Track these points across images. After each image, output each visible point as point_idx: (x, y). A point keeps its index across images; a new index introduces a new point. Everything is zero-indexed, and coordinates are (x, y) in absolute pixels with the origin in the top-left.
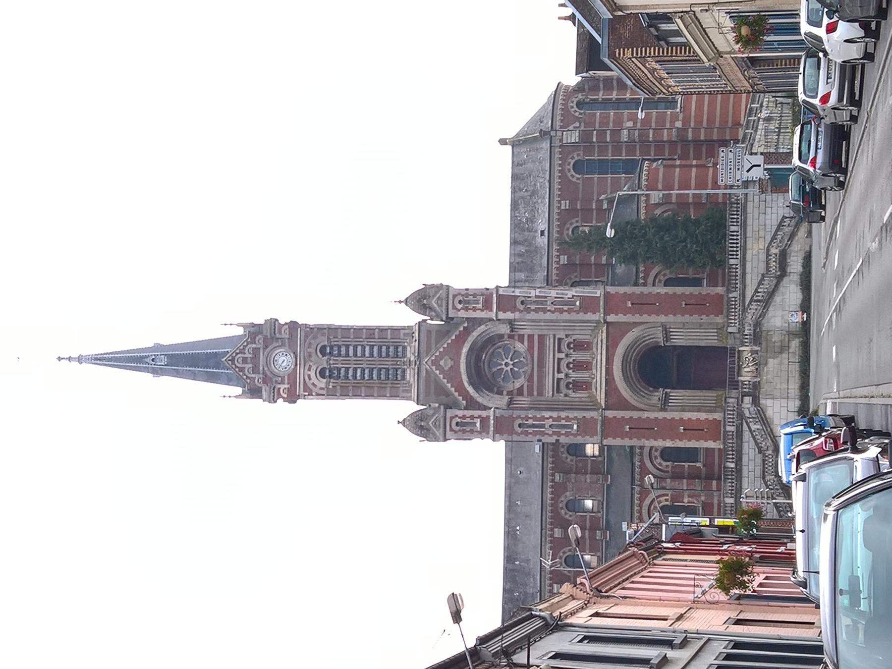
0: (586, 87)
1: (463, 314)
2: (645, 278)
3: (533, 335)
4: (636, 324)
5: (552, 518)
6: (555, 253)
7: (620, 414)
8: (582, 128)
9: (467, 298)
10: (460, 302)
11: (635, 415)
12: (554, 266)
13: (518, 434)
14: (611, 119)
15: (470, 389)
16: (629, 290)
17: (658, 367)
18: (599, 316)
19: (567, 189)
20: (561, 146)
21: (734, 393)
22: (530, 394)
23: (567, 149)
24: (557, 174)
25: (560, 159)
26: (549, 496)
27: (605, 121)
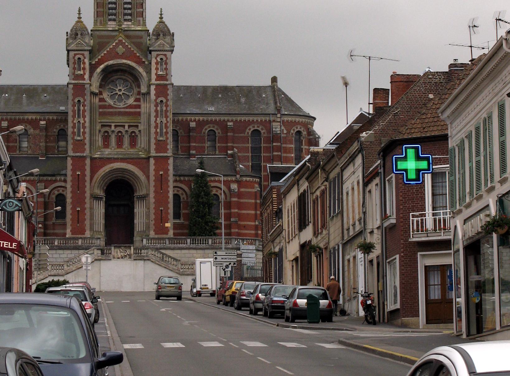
0: (311, 137)
1: (154, 61)
2: (181, 181)
3: (140, 108)
4: (148, 177)
5: (15, 119)
6: (197, 118)
7: (88, 168)
8: (282, 135)
9: (165, 63)
10: (161, 59)
11: (88, 178)
12: (189, 118)
13: (73, 100)
14: (288, 155)
15: (102, 66)
16: (171, 172)
17: (120, 194)
18: (153, 153)
19: (241, 126)
20: (270, 121)
21: (103, 243)
22: (101, 107)
23: (268, 125)
24: (251, 119)
25: (261, 121)
26: (30, 118)
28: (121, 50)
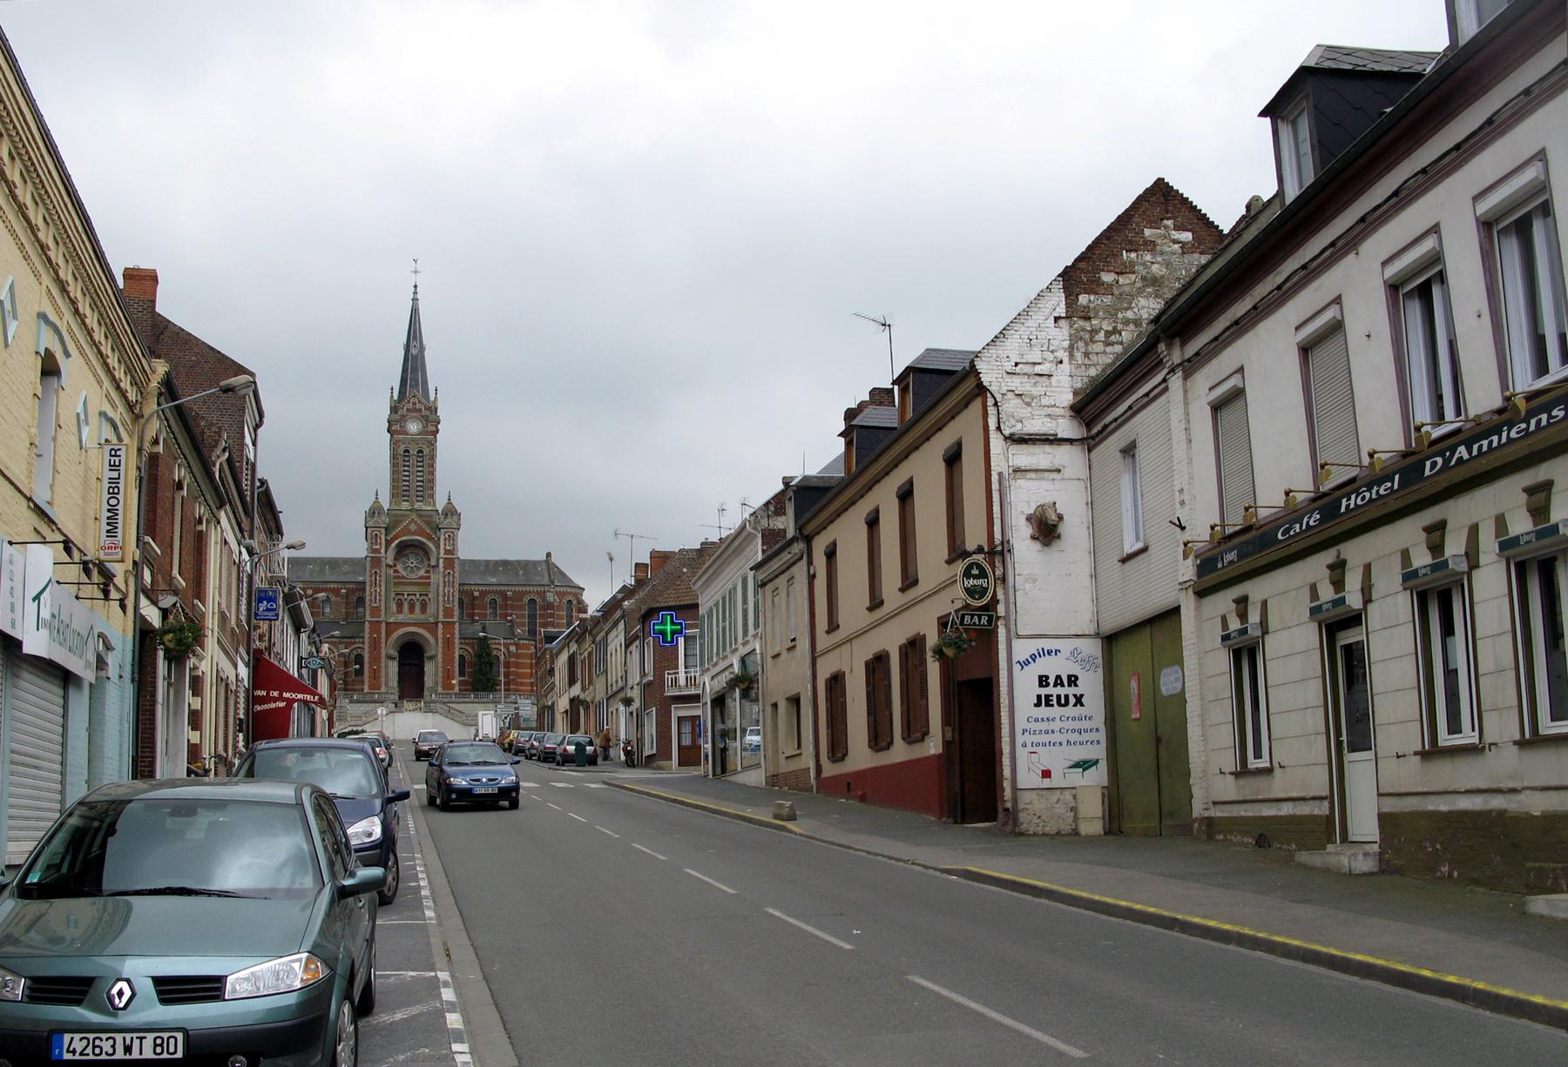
9: (452, 539)
17: (412, 655)
18: (441, 618)
27: (560, 617)
28: (413, 527)
